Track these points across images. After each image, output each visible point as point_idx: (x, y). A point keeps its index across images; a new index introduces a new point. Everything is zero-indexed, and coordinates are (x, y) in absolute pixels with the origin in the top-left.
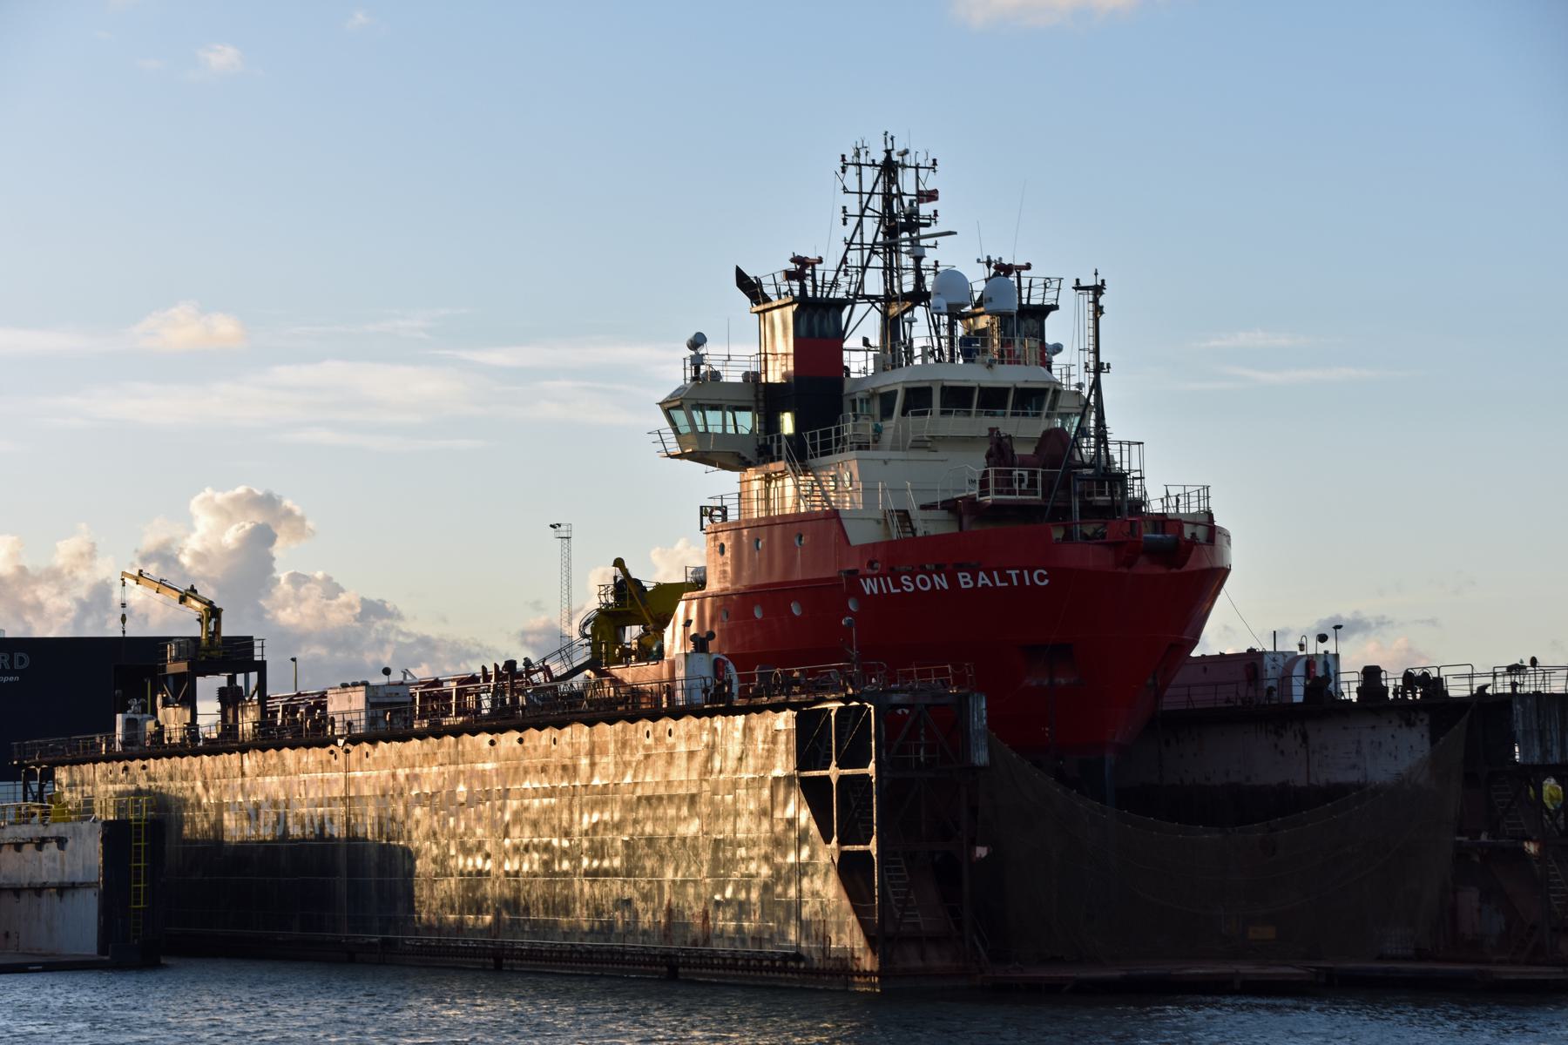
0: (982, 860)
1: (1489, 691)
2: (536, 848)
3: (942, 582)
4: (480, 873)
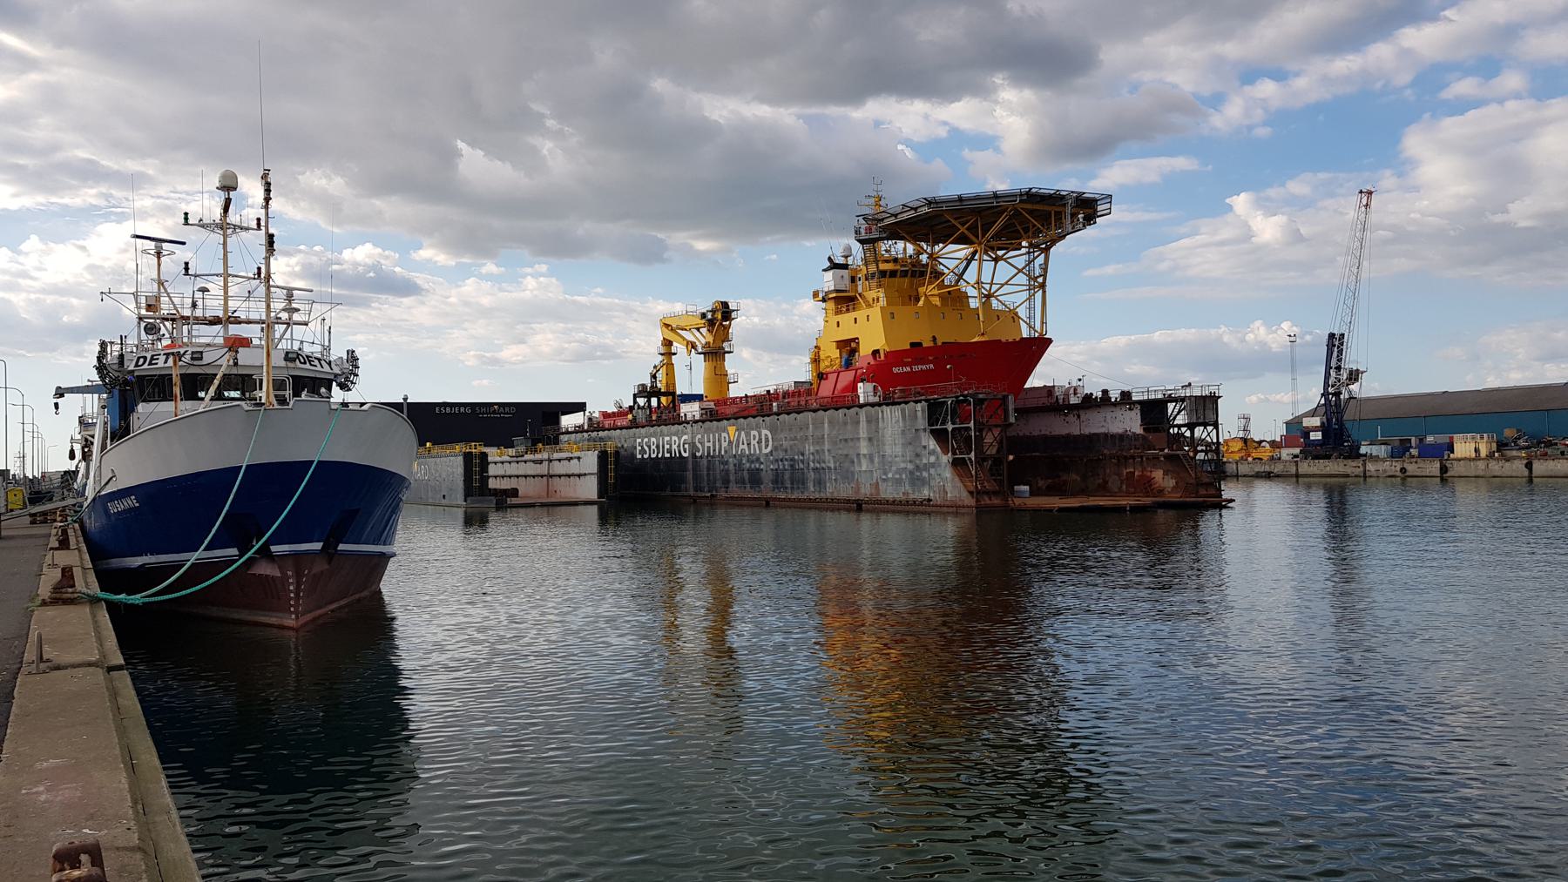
0: (1012, 461)
1: (1173, 396)
2: (786, 460)
3: (909, 369)
4: (758, 469)
